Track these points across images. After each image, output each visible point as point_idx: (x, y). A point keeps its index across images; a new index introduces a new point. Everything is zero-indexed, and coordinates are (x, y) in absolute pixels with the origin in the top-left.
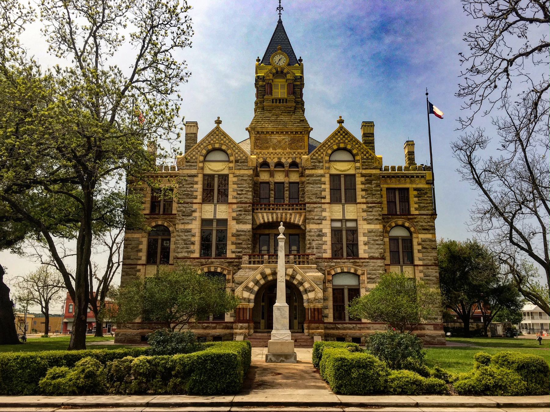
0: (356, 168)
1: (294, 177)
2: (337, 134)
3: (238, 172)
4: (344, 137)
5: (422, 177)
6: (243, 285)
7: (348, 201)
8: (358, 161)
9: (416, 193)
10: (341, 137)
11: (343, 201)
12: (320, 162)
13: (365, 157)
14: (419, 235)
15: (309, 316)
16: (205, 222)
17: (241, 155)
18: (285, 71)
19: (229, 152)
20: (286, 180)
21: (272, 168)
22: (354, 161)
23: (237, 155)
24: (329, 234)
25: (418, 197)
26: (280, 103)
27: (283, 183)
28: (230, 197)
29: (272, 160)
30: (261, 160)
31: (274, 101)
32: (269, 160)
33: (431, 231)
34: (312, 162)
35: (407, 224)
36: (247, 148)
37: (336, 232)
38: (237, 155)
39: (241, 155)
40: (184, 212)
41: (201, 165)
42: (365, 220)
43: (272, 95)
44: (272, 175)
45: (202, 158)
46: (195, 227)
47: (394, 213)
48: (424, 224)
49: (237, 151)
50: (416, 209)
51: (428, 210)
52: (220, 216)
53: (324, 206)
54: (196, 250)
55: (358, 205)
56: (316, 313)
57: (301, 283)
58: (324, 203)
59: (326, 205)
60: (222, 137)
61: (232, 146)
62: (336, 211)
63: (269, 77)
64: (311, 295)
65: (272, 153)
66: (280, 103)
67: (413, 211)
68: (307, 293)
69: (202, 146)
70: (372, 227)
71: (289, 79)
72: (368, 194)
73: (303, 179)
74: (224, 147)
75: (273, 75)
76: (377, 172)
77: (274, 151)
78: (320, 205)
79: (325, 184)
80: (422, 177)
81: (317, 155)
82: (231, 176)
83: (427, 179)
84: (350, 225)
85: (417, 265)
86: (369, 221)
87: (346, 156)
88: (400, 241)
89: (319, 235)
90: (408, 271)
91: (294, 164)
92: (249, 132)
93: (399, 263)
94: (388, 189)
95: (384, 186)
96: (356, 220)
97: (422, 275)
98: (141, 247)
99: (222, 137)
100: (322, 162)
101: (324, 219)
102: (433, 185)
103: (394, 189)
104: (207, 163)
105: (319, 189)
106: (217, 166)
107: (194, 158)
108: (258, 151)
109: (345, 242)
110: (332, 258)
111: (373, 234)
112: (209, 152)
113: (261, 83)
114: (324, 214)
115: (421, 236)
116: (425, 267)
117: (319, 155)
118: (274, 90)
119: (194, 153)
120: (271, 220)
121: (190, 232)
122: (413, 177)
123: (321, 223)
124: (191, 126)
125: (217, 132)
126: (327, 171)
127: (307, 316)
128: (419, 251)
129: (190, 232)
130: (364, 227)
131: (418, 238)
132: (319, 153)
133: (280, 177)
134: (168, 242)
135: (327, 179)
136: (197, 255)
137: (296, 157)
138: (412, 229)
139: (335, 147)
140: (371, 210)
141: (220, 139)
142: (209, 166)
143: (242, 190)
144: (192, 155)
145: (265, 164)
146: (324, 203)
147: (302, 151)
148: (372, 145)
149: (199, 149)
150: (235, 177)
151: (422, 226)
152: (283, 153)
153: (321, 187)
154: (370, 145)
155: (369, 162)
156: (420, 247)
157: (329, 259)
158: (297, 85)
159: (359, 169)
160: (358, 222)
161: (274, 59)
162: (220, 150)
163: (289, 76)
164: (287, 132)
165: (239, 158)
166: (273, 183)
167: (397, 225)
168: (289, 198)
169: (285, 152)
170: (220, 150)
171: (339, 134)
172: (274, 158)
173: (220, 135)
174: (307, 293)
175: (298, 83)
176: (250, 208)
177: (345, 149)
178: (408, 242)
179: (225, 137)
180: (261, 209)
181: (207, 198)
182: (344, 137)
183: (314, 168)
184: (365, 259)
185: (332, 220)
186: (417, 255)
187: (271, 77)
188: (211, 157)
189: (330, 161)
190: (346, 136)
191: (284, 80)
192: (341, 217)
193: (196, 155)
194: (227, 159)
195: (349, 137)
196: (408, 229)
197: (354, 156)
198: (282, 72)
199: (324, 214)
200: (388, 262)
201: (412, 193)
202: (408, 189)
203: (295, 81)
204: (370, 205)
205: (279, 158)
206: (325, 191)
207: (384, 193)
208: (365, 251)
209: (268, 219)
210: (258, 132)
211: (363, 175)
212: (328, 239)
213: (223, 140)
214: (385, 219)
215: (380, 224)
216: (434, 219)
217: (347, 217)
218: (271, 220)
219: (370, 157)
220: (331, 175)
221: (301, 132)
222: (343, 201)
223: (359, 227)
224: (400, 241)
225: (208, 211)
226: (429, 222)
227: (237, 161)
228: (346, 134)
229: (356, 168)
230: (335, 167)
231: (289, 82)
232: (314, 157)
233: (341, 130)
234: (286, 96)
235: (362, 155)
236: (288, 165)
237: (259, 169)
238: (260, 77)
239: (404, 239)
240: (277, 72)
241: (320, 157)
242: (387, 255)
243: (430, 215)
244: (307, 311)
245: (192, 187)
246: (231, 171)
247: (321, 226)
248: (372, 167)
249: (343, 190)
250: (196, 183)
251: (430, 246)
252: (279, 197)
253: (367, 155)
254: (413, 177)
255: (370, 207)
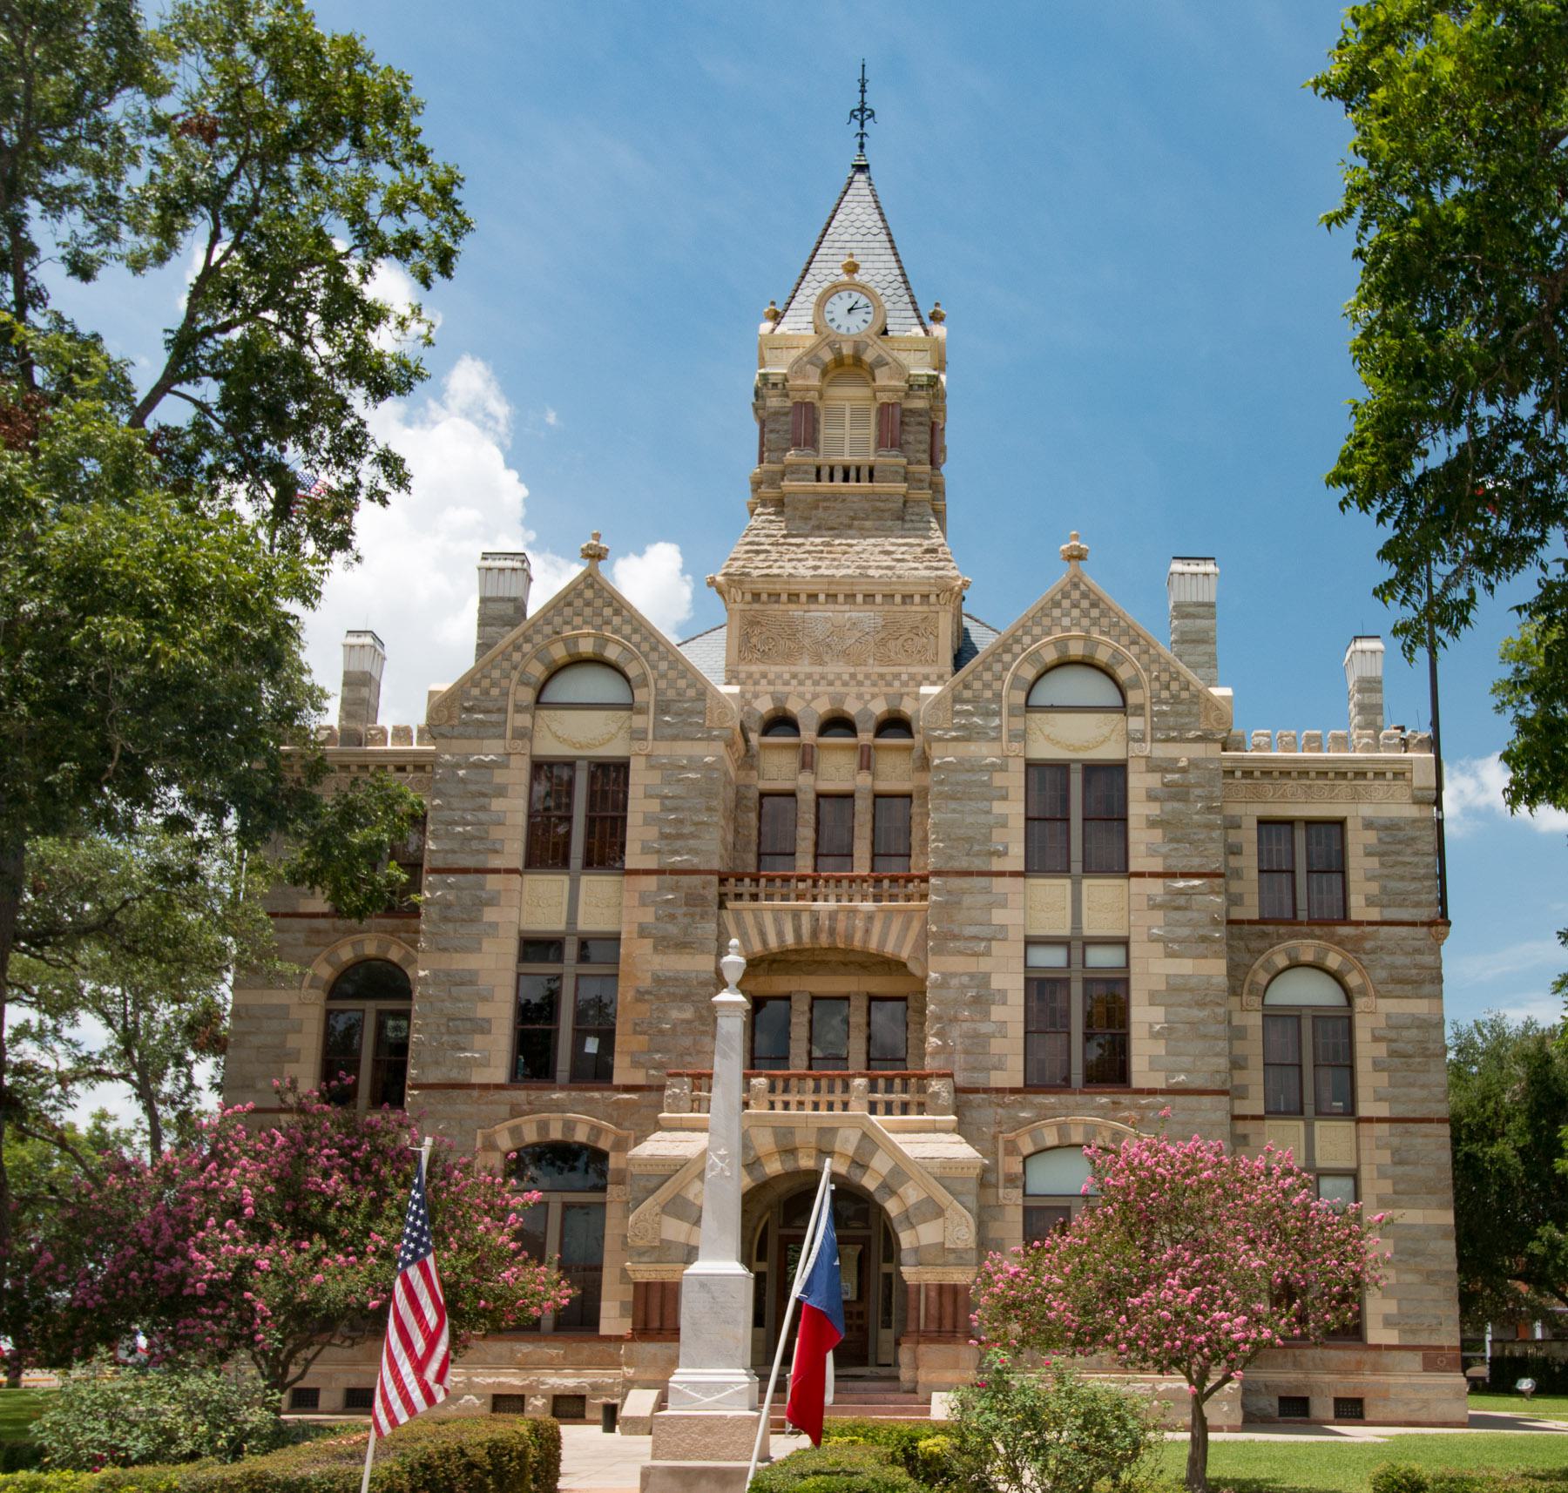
0: (1130, 738)
1: (894, 773)
2: (1057, 604)
3: (663, 749)
4: (1085, 614)
5: (1398, 775)
6: (664, 1193)
7: (1092, 868)
8: (1139, 710)
9: (1371, 837)
10: (1076, 613)
11: (1076, 867)
12: (989, 714)
13: (1165, 694)
14: (1381, 1002)
15: (923, 1311)
16: (536, 948)
17: (682, 683)
18: (869, 357)
19: (632, 671)
20: (863, 782)
21: (808, 735)
22: (1123, 708)
23: (663, 684)
24: (1017, 997)
25: (1381, 855)
26: (846, 479)
27: (849, 796)
28: (632, 847)
29: (809, 707)
30: (764, 706)
31: (825, 473)
32: (794, 707)
33: (1428, 988)
34: (958, 713)
35: (1333, 961)
36: (709, 659)
37: (1041, 988)
38: (663, 684)
39: (682, 683)
40: (449, 906)
41: (523, 720)
42: (1154, 939)
43: (817, 450)
44: (807, 761)
45: (527, 695)
46: (495, 973)
47: (1288, 915)
48: (1400, 960)
49: (663, 666)
50: (1370, 902)
51: (1417, 905)
52: (592, 920)
53: (1000, 884)
54: (493, 1056)
55: (1133, 880)
56: (948, 1301)
57: (889, 1189)
58: (1001, 874)
59: (1007, 880)
60: (608, 611)
61: (645, 647)
62: (1047, 904)
63: (805, 377)
64: (928, 1233)
65: (809, 676)
66: (846, 479)
67: (1359, 908)
68: (913, 1226)
69: (527, 647)
70: (1185, 966)
71: (884, 389)
72: (1171, 840)
73: (929, 779)
74: (612, 653)
75: (824, 373)
76: (1211, 755)
77: (818, 669)
78: (983, 881)
79: (1005, 798)
80: (1398, 775)
81: (977, 685)
82: (636, 766)
83: (1416, 783)
84: (1100, 958)
85: (1369, 1120)
86: (1171, 947)
87: (1096, 690)
88: (1307, 1025)
89: (977, 1000)
90: (1334, 1142)
91: (895, 724)
92: (720, 592)
93: (1302, 1113)
94: (1263, 822)
95: (1251, 812)
96: (1124, 942)
97: (1385, 1157)
98: (293, 1041)
99: (608, 611)
100: (998, 714)
101: (1000, 934)
102: (1440, 808)
103: (1290, 822)
104: (544, 713)
105: (982, 819)
106: (580, 733)
107: (495, 692)
108: (754, 668)
109: (1084, 1031)
110: (1029, 1088)
111: (1187, 996)
112: (555, 671)
113: (774, 402)
114: (999, 916)
115: (1388, 1006)
116: (1400, 1127)
117: (987, 686)
118: (825, 432)
119: (496, 674)
120: (790, 940)
121: (472, 983)
122: (1360, 775)
123: (987, 953)
124: (502, 570)
125: (589, 594)
126: (1016, 747)
127: (912, 1314)
128: (1377, 1066)
129: (472, 983)
130: (1151, 971)
131: (1374, 1016)
132: (987, 676)
133: (838, 770)
134: (404, 1023)
135: (1015, 780)
136: (499, 1073)
137: (902, 696)
138: (1353, 980)
139: (1050, 656)
140: (1182, 901)
141: (599, 621)
142: (554, 726)
143: (680, 822)
144: (486, 683)
145: (781, 722)
146: (1001, 874)
147: (926, 670)
148: (1208, 648)
149: (516, 656)
150: (652, 767)
151: (1393, 967)
152: (853, 676)
153: (989, 812)
154: (1202, 648)
155: (1178, 714)
156: (1381, 1050)
157: (1014, 1091)
158: (912, 412)
159: (1142, 740)
160: (1133, 947)
161: (828, 307)
162: (598, 661)
163: (883, 378)
164: (869, 597)
165: (671, 694)
166: (812, 796)
167: (1295, 965)
168: (816, 856)
169: (861, 672)
170: (598, 661)
171: (1066, 603)
172: (815, 696)
173: (598, 603)
174: (913, 1226)
175: (919, 404)
176: (712, 892)
177: (1087, 663)
178: (1337, 1028)
179: (617, 612)
180: (755, 897)
181: (546, 850)
182: (1085, 614)
183: (969, 734)
184: (1152, 1092)
185: (1030, 942)
186: (1368, 1079)
187: (814, 381)
188: (565, 689)
189: (1029, 707)
190: (1095, 613)
191: (863, 392)
192: (1065, 930)
193: (504, 683)
194: (626, 699)
195: (1103, 614)
196: (1337, 977)
197: (1121, 689)
198: (857, 360)
199: (999, 916)
200: (1256, 1105)
201: (1358, 840)
202: (1341, 823)
203: (907, 396)
204: (1181, 884)
205: (841, 698)
206: (1004, 826)
207: (1248, 836)
208: (1154, 1063)
209: (780, 934)
210: (756, 597)
211: (1154, 766)
212: (1011, 1013)
213: (608, 623)
214: (1244, 937)
215: (1216, 955)
216: (1439, 940)
217: (1088, 931)
218: (790, 940)
219: (1185, 695)
220: (1030, 765)
221: (925, 597)
222: (1076, 867)
223: (1135, 968)
224: (1307, 1025)
225: (544, 903)
226: (1417, 951)
227: (663, 708)
228: (1094, 605)
229: (1130, 738)
230: (1048, 730)
231: (884, 397)
232: (967, 694)
233: (1076, 586)
234: (871, 458)
235: (1156, 685)
236: (872, 725)
237: (754, 738)
238: (772, 379)
239: (1321, 1016)
240: (839, 361)
241: (988, 694)
242: (1254, 1078)
243: (1423, 924)
244: (912, 1296)
245: (483, 808)
246: (636, 746)
247: (984, 965)
248: (1191, 734)
249: (1078, 816)
250: (501, 792)
251: (1417, 1046)
252: (830, 850)
253: (1174, 686)
254: (1360, 775)
255: (1181, 892)
